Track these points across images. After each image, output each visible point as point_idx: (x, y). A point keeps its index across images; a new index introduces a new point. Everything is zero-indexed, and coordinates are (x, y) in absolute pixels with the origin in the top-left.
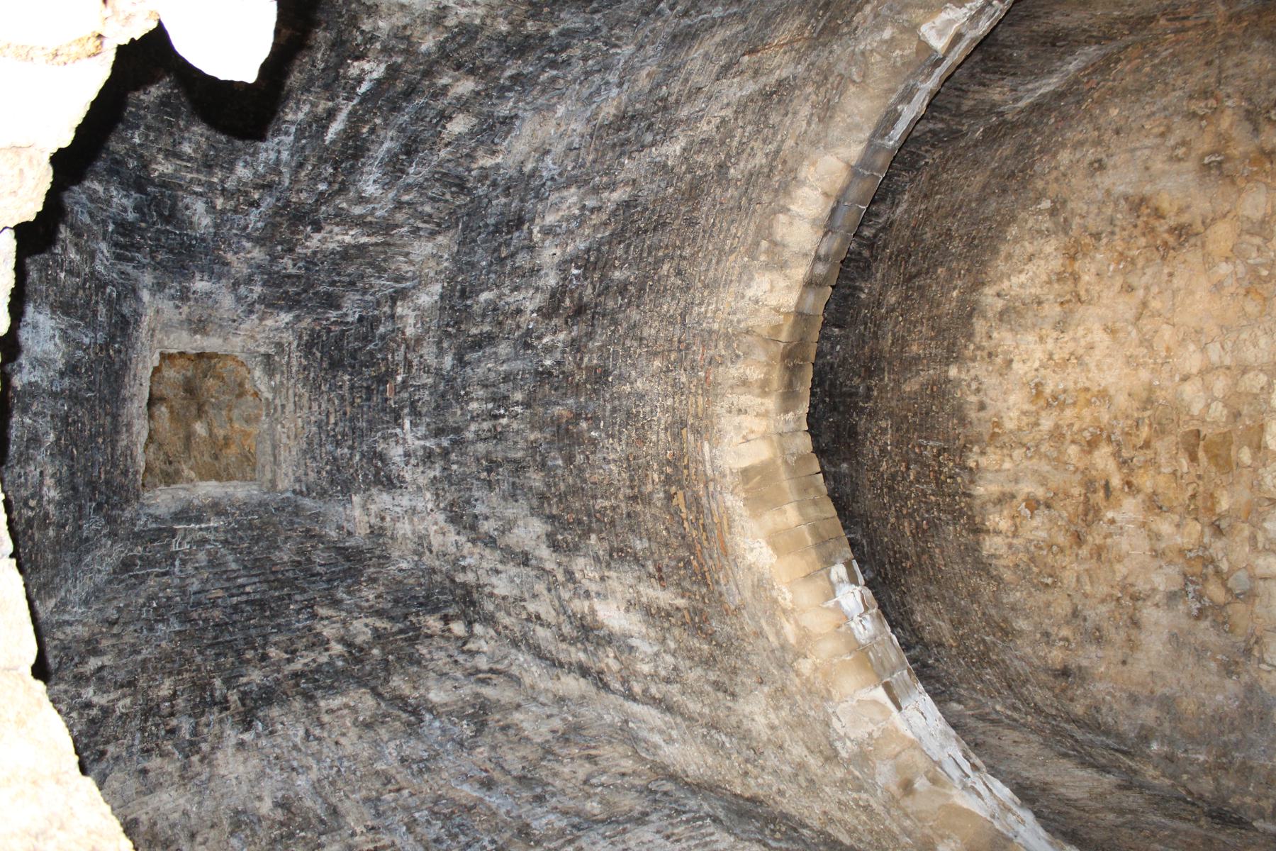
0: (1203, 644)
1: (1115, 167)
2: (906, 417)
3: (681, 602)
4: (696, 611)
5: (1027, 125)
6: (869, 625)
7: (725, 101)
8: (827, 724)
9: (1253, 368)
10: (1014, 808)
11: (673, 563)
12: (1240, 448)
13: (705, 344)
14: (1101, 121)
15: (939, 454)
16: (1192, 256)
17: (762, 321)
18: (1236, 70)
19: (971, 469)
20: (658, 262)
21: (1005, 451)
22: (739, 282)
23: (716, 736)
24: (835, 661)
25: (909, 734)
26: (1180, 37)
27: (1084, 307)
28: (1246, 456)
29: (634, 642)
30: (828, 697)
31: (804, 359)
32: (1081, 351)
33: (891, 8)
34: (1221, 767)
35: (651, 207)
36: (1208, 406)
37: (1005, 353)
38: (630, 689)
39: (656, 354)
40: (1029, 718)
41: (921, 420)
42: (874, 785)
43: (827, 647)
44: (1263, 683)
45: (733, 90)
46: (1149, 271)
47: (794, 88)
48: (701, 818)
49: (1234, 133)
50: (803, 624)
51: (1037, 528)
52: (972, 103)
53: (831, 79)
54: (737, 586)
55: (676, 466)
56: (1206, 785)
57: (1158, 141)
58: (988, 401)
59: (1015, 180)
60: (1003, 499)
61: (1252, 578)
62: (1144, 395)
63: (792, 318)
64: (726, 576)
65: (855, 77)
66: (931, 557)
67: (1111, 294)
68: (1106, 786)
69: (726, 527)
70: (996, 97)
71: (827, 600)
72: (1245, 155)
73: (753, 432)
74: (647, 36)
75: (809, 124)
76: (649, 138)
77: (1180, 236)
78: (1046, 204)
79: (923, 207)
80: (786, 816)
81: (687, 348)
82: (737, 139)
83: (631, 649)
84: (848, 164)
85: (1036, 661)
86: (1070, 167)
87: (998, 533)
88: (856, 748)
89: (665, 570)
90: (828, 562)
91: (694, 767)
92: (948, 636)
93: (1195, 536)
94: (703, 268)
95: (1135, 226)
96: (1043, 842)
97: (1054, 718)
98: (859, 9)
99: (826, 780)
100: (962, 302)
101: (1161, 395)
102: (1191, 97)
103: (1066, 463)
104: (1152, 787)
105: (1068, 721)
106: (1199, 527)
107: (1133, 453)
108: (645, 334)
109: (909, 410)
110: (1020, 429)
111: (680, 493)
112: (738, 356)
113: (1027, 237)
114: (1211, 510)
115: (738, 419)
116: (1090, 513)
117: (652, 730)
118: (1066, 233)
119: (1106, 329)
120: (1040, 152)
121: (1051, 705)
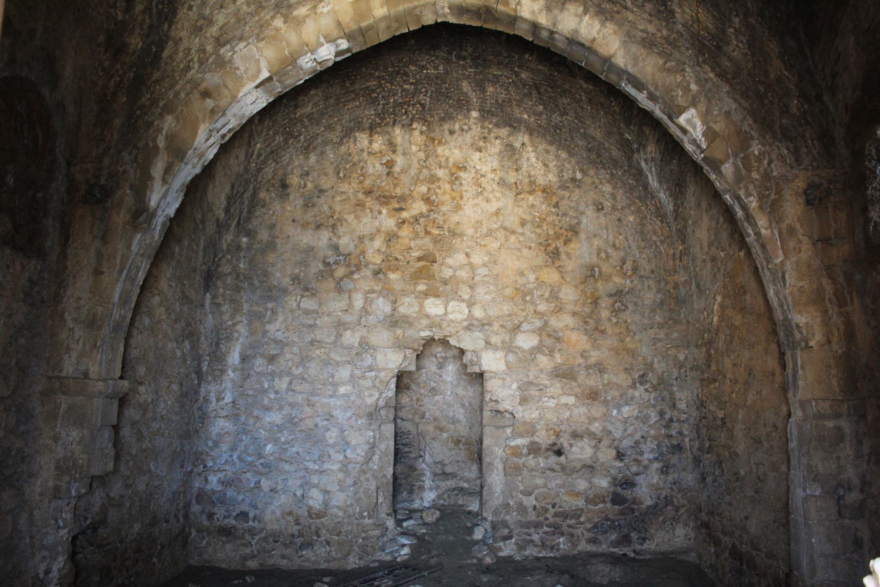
0: (309, 265)
1: (598, 217)
2: (446, 83)
5: (630, 166)
6: (309, 65)
8: (241, 39)
9: (472, 292)
12: (426, 284)
14: (627, 210)
15: (421, 104)
18: (646, 286)
19: (411, 125)
21: (423, 147)
24: (284, 43)
25: (241, 94)
27: (514, 197)
28: (421, 287)
30: (259, 39)
31: (485, 21)
32: (485, 194)
33: (709, 90)
34: (238, 276)
36: (451, 267)
37: (486, 148)
40: (254, 165)
42: (204, 72)
44: (289, 297)
47: (667, 22)
50: (307, 20)
51: (374, 167)
52: (647, 133)
56: (226, 268)
57: (611, 243)
58: (455, 136)
59: (596, 157)
60: (392, 146)
61: (350, 291)
62: (458, 232)
63: (513, 14)
65: (668, 64)
66: (353, 100)
67: (520, 213)
68: (217, 212)
70: (649, 149)
71: (325, 37)
72: (597, 290)
75: (642, 31)
78: (579, 176)
79: (583, 98)
80: (174, 12)
84: (613, 56)
85: (290, 168)
86: (600, 191)
87: (371, 142)
88: (227, 59)
90: (349, 37)
92: (302, 112)
93: (373, 260)
95: (561, 228)
97: (256, 180)
98: (713, 70)
99: (203, 39)
100: (520, 121)
101: (457, 241)
102: (634, 262)
103: (416, 185)
104: (220, 238)
105: (254, 188)
106: (378, 262)
109: (450, 85)
110: (437, 156)
114: (389, 269)
116: (385, 199)
118: (559, 187)
119: (499, 209)
120: (612, 173)
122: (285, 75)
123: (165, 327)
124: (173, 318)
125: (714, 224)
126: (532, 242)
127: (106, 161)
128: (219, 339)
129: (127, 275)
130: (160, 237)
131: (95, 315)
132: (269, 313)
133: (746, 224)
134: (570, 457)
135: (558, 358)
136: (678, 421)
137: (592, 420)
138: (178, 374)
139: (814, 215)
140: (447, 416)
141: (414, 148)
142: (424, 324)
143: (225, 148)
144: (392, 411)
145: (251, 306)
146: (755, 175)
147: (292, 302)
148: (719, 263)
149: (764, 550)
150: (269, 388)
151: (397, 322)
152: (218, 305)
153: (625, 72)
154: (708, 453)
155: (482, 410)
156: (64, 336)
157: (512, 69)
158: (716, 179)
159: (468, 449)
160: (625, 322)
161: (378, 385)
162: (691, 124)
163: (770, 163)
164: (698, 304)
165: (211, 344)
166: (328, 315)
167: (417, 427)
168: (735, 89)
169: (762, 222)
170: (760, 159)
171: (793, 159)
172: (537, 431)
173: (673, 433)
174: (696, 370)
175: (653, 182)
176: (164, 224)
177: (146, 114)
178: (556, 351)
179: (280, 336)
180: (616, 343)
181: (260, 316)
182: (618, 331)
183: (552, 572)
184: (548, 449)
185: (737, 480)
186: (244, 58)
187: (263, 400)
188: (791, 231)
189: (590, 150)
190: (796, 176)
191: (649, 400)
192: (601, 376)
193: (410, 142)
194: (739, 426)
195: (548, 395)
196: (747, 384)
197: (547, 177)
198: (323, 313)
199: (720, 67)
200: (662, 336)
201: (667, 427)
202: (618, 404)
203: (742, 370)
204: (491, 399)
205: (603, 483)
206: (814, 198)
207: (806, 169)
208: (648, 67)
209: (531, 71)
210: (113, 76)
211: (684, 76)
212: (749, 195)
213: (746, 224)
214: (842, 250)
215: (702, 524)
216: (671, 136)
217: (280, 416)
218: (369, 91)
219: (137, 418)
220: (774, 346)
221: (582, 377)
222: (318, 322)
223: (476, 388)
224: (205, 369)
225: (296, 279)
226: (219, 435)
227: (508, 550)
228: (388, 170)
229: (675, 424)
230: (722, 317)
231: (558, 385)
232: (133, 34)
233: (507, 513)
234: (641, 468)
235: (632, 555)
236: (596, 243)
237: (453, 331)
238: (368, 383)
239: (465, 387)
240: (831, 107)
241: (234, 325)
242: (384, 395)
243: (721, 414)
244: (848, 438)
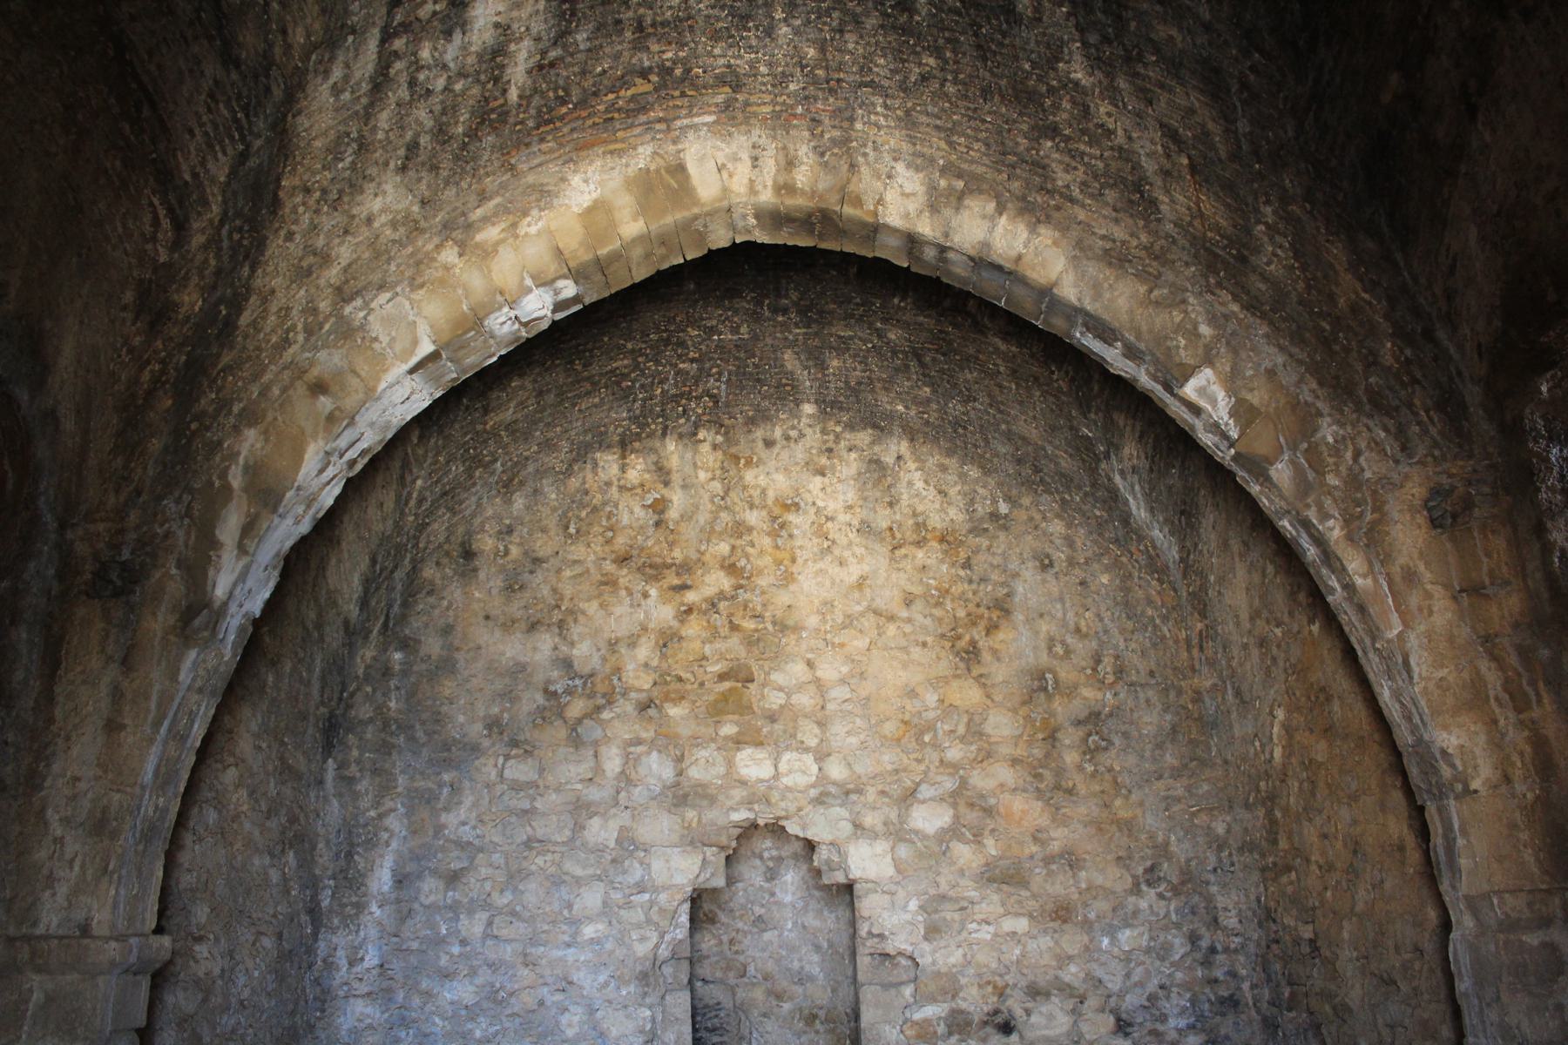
0: (518, 698)
1: (1044, 581)
3: (513, 94)
4: (504, 114)
5: (1093, 485)
6: (506, 328)
7: (1135, 135)
8: (381, 287)
9: (824, 732)
10: (312, 512)
11: (561, 82)
12: (736, 723)
13: (836, 113)
14: (1096, 566)
16: (944, 667)
17: (866, 183)
19: (695, 434)
20: (937, 52)
21: (718, 472)
22: (914, 154)
23: (350, 151)
25: (383, 385)
26: (1182, 644)
28: (728, 730)
29: (457, 37)
30: (415, 285)
31: (821, 237)
32: (837, 552)
35: (1007, 42)
36: (781, 689)
37: (833, 468)
38: (396, 34)
39: (823, 50)
40: (411, 518)
41: (751, 374)
42: (316, 348)
43: (476, 281)
44: (482, 760)
45: (1148, 144)
46: (928, 621)
48: (243, 139)
49: (1077, 702)
50: (501, 249)
51: (632, 513)
52: (1121, 423)
53: (1155, 264)
54: (540, 165)
55: (683, 80)
56: (364, 711)
57: (1072, 626)
58: (776, 450)
59: (1032, 473)
60: (663, 474)
61: (596, 743)
62: (791, 623)
63: (870, 220)
64: (551, 151)
65: (1156, 293)
66: (588, 393)
68: (345, 607)
69: (612, 147)
70: (1126, 451)
71: (533, 277)
72: (1053, 714)
73: (731, 176)
74: (1219, 36)
75: (1103, 237)
76: (1093, 38)
77: (967, 652)
78: (1004, 508)
79: (1002, 369)
80: (261, 245)
81: (832, 91)
82: (1088, 150)
83: (448, 34)
84: (1055, 284)
86: (1044, 533)
87: (623, 469)
89: (552, 72)
90: (577, 275)
91: (307, 125)
93: (637, 684)
94: (930, 109)
95: (978, 605)
96: (278, 547)
98: (1236, 298)
99: (313, 290)
100: (891, 416)
101: (789, 640)
102: (1117, 657)
103: (708, 541)
104: (352, 655)
105: (413, 560)
106: (646, 687)
107: (725, 613)
108: (847, 36)
109: (761, 359)
110: (745, 488)
111: (648, 87)
112: (822, 154)
113: (966, 488)
115: (745, 156)
116: (653, 570)
117: (347, 66)
118: (970, 531)
119: (863, 578)
120: (1063, 500)
121: (429, 542)
122: (462, 347)
123: (247, 826)
124: (264, 808)
125: (1257, 578)
127: (133, 517)
128: (352, 845)
129: (170, 730)
130: (234, 655)
131: (105, 810)
132: (445, 791)
133: (1324, 571)
134: (1030, 1035)
135: (992, 847)
136: (1226, 950)
137: (1064, 960)
138: (274, 916)
139: (1449, 545)
140: (788, 969)
141: (702, 475)
142: (737, 799)
143: (356, 487)
144: (685, 965)
145: (412, 779)
146: (1332, 480)
147: (487, 768)
148: (1275, 651)
150: (449, 934)
151: (686, 796)
152: (351, 781)
153: (1080, 311)
154: (1290, 1010)
155: (853, 954)
156: (42, 854)
157: (871, 325)
158: (1261, 492)
159: (832, 1031)
160: (1110, 770)
161: (655, 918)
162: (1208, 398)
163: (1357, 454)
165: (337, 855)
166: (558, 790)
167: (734, 994)
168: (1278, 329)
169: (1355, 564)
170: (1338, 450)
172: (961, 988)
173: (1219, 974)
174: (1251, 851)
175: (1139, 511)
176: (242, 629)
177: (208, 429)
178: (987, 832)
179: (467, 833)
180: (1096, 811)
181: (429, 798)
182: (1097, 788)
186: (388, 321)
187: (438, 957)
188: (1410, 576)
189: (1019, 461)
190: (1407, 477)
191: (1167, 915)
192: (1074, 876)
193: (695, 464)
194: (1347, 953)
195: (978, 917)
196: (1353, 872)
197: (947, 514)
198: (547, 787)
199: (1248, 293)
200: (1180, 792)
201: (1207, 963)
202: (1111, 926)
203: (1339, 845)
204: (870, 933)
206: (1446, 514)
208: (1120, 299)
209: (906, 326)
210: (148, 362)
211: (1186, 312)
212: (1325, 516)
213: (1324, 571)
214: (1508, 605)
216: (1172, 421)
217: (471, 988)
218: (618, 377)
219: (190, 1008)
220: (1397, 797)
221: (1038, 878)
222: (538, 805)
223: (840, 913)
224: (325, 903)
225: (494, 725)
226: (353, 1031)
228: (656, 517)
229: (1220, 958)
231: (995, 897)
232: (185, 287)
236: (1044, 628)
237: (792, 808)
238: (638, 915)
239: (819, 912)
240: (1452, 351)
241: (380, 816)
242: (667, 938)
243: (1307, 932)
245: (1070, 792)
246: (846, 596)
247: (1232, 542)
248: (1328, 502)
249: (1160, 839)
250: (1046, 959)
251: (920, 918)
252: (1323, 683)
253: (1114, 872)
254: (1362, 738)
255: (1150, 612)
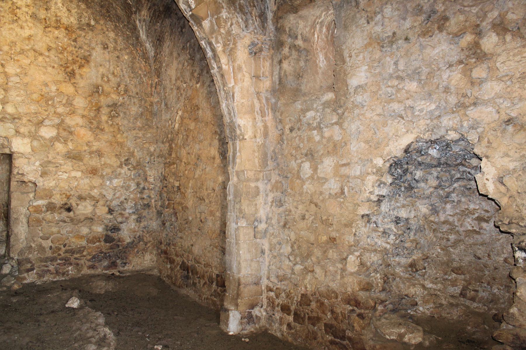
1: (104, 53)
5: (128, 22)
9: (6, 94)
14: (124, 52)
16: (61, 77)
26: (149, 85)
32: (20, 22)
46: (56, 59)
49: (109, 99)
57: (111, 72)
67: (47, 41)
70: (143, 13)
72: (100, 101)
77: (70, 73)
78: (93, 23)
95: (77, 57)
102: (126, 86)
113: (79, 11)
118: (78, 28)
120: (116, 25)
125: (180, 66)
126: (55, 63)
133: (212, 61)
134: (77, 212)
135: (71, 146)
136: (148, 189)
137: (93, 188)
139: (253, 61)
148: (182, 91)
149: (203, 263)
154: (167, 208)
158: (197, 30)
163: (232, 25)
164: (165, 116)
171: (244, 25)
172: (53, 195)
173: (145, 196)
174: (161, 157)
175: (143, 36)
178: (69, 140)
182: (112, 130)
183: (66, 290)
184: (61, 208)
185: (187, 223)
188: (240, 68)
190: (245, 36)
191: (131, 175)
192: (99, 159)
195: (63, 170)
196: (196, 165)
200: (140, 135)
202: (110, 177)
203: (193, 156)
205: (99, 229)
207: (250, 33)
212: (217, 42)
213: (212, 61)
215: (161, 252)
221: (86, 159)
227: (30, 278)
229: (146, 191)
230: (181, 124)
231: (70, 164)
233: (30, 253)
234: (124, 219)
235: (118, 274)
243: (177, 184)
244: (261, 193)
245: (102, 130)
246: (22, 42)
247: (174, 53)
248: (219, 38)
249: (131, 150)
250: (87, 187)
251: (40, 169)
252: (197, 104)
253: (114, 159)
254: (207, 123)
255: (140, 72)
